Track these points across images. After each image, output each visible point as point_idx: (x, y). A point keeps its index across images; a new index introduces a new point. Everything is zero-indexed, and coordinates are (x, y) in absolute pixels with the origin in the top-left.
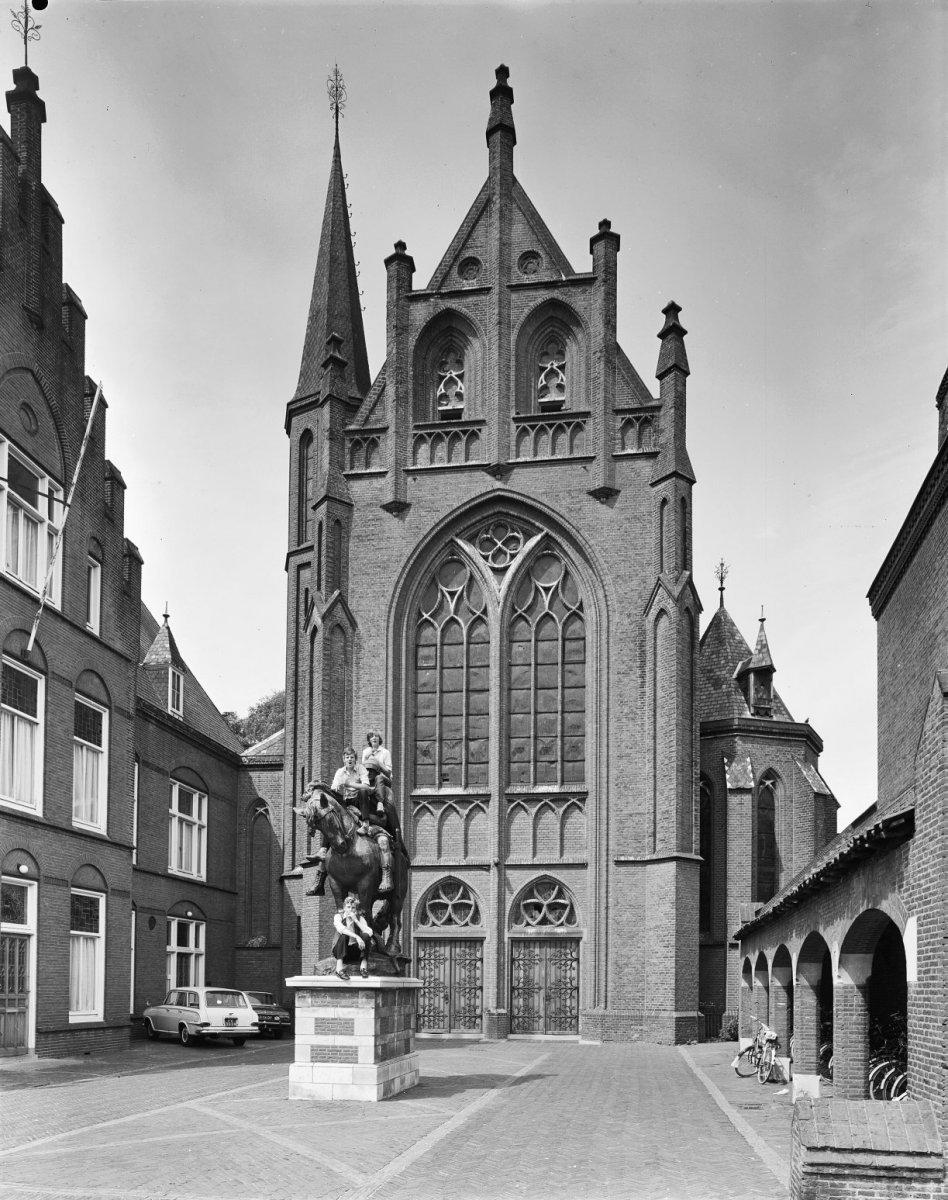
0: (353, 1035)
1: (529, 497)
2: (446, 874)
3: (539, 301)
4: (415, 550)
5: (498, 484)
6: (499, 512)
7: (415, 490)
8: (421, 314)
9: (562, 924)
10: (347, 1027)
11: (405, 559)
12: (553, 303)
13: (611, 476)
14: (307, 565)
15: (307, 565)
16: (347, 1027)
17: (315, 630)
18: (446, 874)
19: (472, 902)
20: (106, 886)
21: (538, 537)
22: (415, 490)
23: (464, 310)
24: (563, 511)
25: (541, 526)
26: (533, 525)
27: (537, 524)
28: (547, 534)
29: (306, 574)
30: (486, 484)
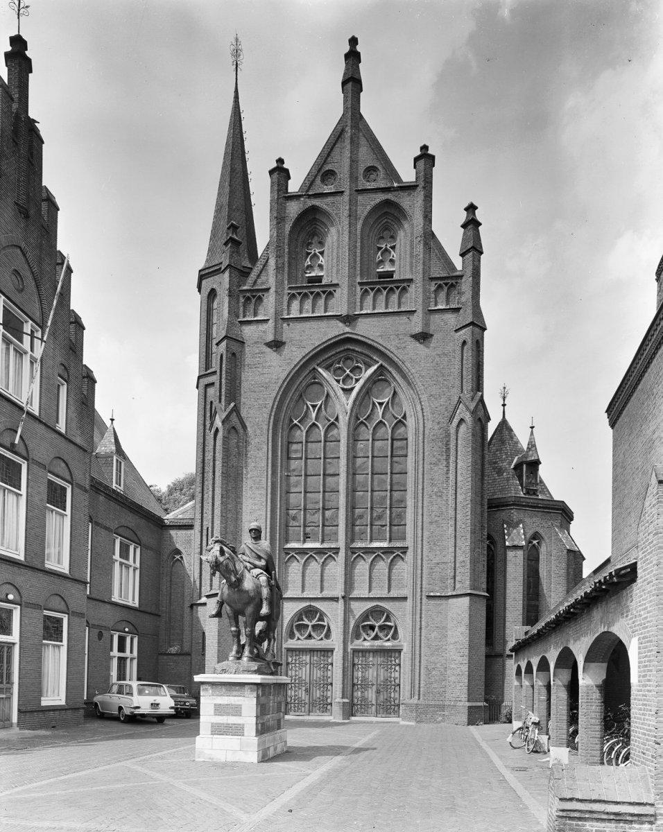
0: (241, 716)
1: (369, 339)
3: (378, 201)
7: (290, 333)
8: (294, 209)
9: (389, 640)
10: (237, 711)
11: (281, 381)
12: (387, 203)
16: (237, 711)
17: (217, 430)
19: (325, 624)
23: (325, 207)
25: (377, 359)
28: (381, 365)
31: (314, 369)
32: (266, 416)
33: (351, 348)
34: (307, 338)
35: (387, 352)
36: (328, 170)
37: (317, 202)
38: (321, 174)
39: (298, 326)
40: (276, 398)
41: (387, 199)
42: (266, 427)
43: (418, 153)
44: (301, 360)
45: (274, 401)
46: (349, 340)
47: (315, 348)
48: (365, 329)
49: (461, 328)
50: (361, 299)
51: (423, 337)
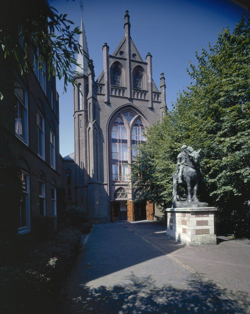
0: (208, 225)
1: (136, 107)
2: (120, 186)
3: (137, 65)
4: (112, 114)
5: (130, 102)
6: (129, 109)
7: (112, 100)
8: (112, 61)
9: (124, 197)
10: (206, 223)
11: (110, 115)
12: (139, 67)
13: (152, 105)
14: (81, 115)
15: (81, 115)
16: (206, 223)
17: (90, 128)
18: (120, 186)
19: (125, 192)
20: (56, 186)
21: (138, 115)
22: (112, 100)
23: (121, 62)
24: (143, 111)
25: (138, 113)
26: (136, 113)
27: (137, 113)
28: (139, 115)
29: (80, 117)
30: (127, 102)
31: (119, 113)
32: (105, 126)
33: (130, 108)
34: (117, 103)
35: (140, 110)
36: (122, 51)
37: (119, 61)
38: (119, 52)
39: (138, 101)
40: (108, 120)
41: (139, 65)
42: (105, 129)
43: (104, 45)
44: (116, 110)
45: (108, 121)
46: (130, 106)
47: (120, 107)
48: (136, 104)
49: (90, 98)
50: (111, 91)
51: (152, 109)
